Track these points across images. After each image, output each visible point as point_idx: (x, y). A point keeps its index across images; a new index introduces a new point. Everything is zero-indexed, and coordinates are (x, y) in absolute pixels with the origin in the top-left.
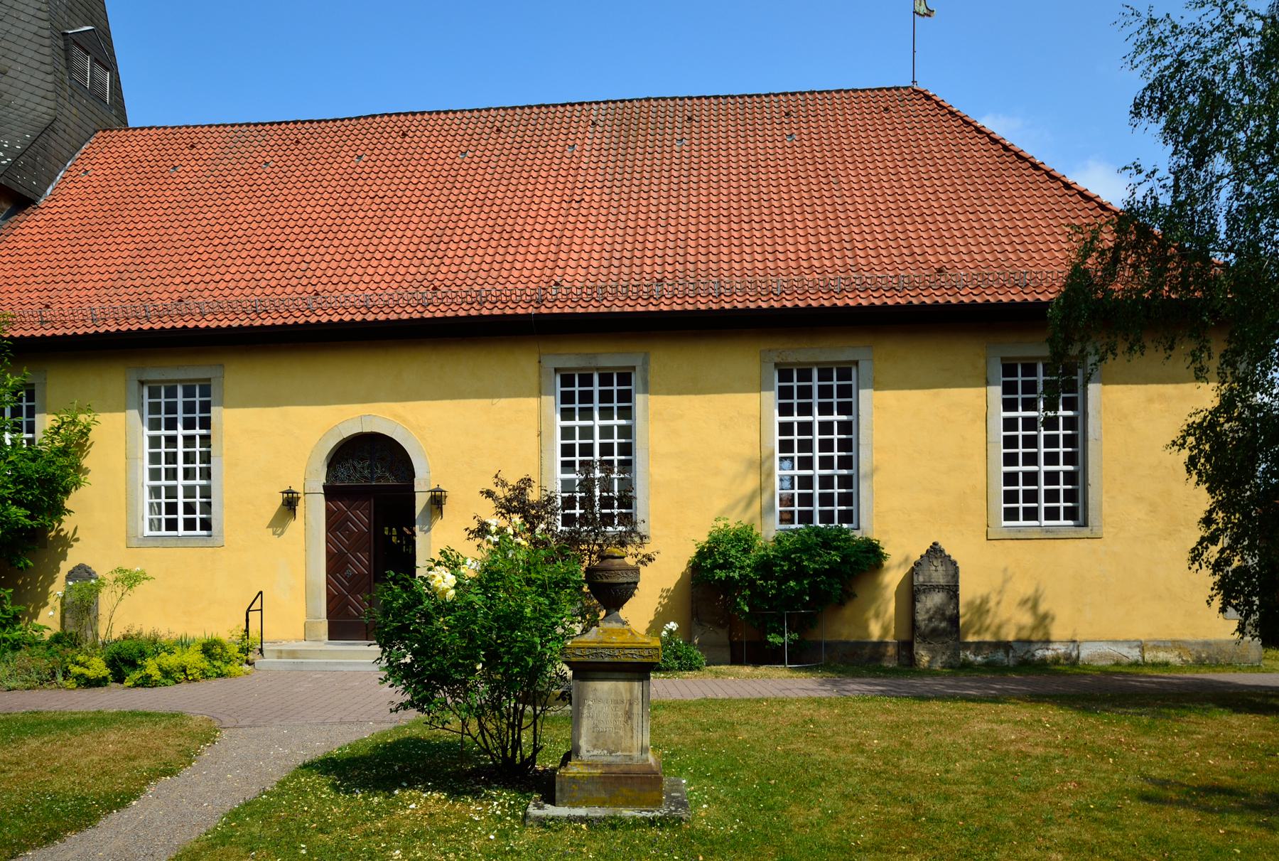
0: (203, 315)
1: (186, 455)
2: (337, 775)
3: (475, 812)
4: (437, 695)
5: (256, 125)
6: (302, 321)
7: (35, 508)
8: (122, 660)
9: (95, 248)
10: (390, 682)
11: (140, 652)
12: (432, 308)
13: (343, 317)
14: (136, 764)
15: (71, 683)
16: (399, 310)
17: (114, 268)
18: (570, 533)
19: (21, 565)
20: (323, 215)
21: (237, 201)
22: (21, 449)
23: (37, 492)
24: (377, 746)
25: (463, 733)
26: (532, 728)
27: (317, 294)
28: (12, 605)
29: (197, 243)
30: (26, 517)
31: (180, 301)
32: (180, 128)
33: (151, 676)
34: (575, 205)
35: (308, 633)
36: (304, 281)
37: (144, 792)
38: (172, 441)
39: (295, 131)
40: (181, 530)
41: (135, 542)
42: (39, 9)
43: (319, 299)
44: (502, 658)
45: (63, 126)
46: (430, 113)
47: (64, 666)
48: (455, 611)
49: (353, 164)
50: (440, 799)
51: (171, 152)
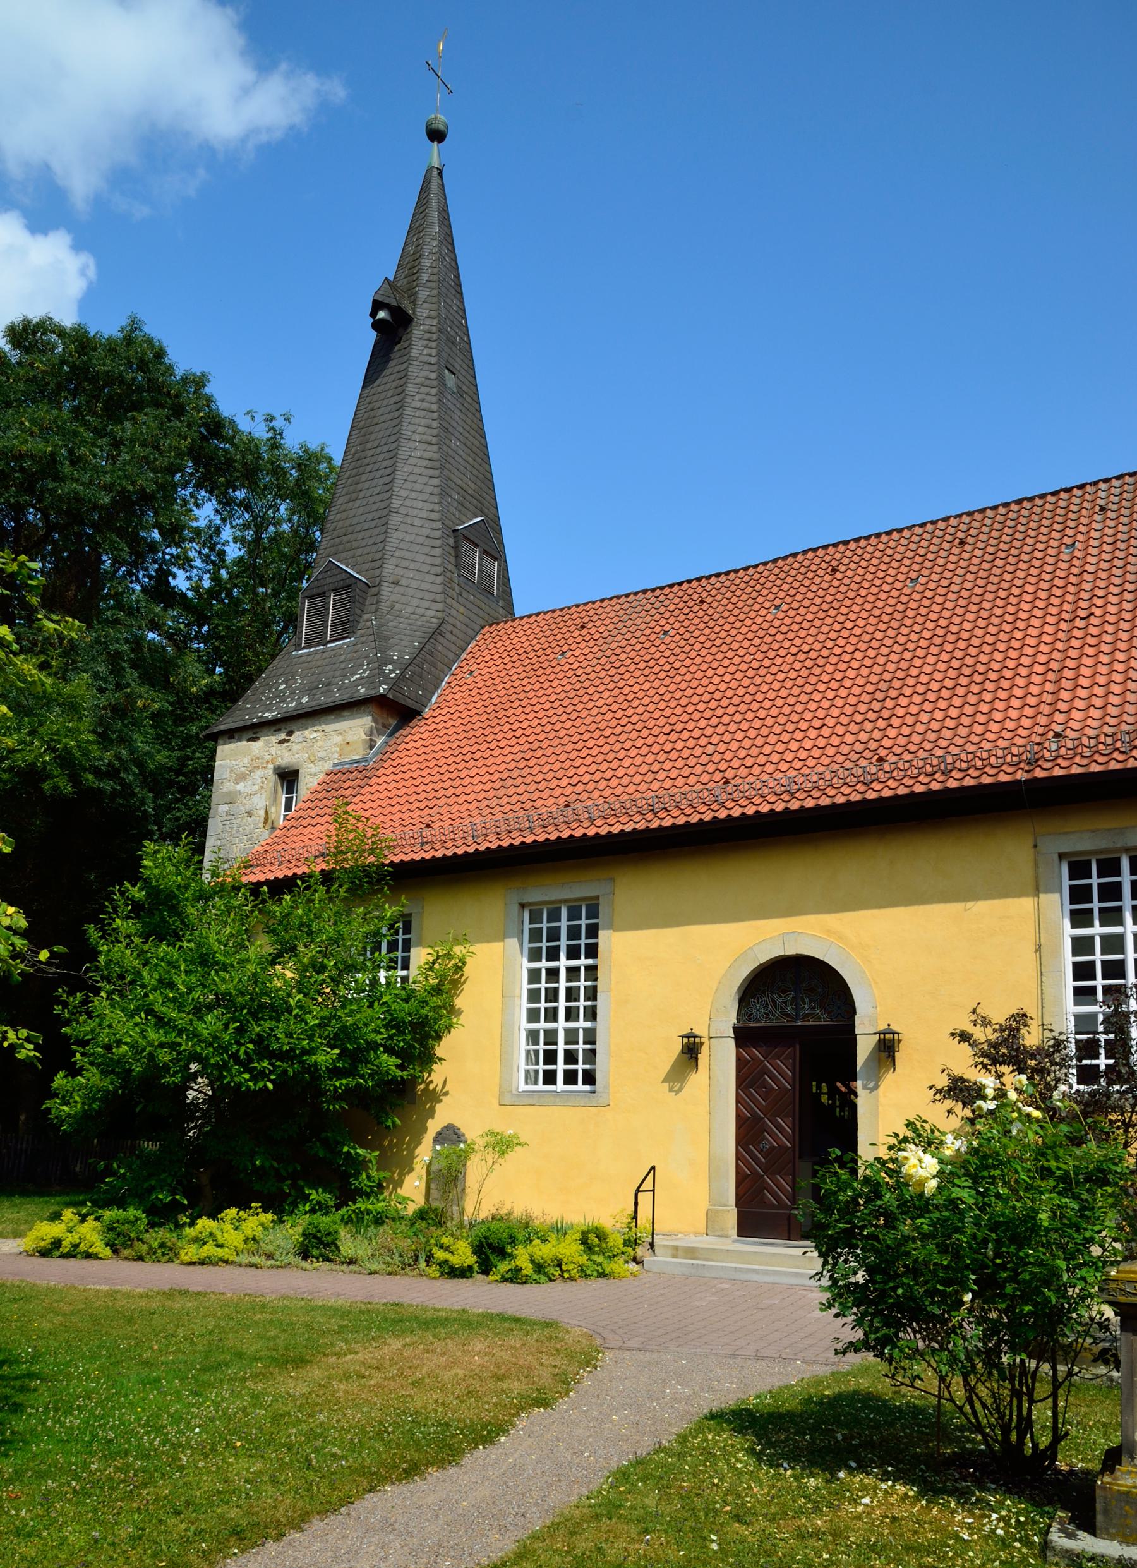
0: (592, 820)
1: (569, 990)
2: (756, 1436)
3: (962, 1524)
4: (901, 1335)
5: (653, 590)
6: (708, 817)
7: (406, 1057)
8: (490, 1246)
9: (478, 755)
10: (835, 1310)
11: (511, 1237)
12: (877, 786)
13: (760, 808)
14: (505, 1385)
15: (434, 1271)
16: (832, 792)
17: (497, 775)
18: (1092, 1094)
19: (389, 1123)
20: (734, 684)
21: (631, 681)
22: (395, 988)
23: (408, 1038)
24: (810, 1399)
25: (939, 1397)
26: (1050, 1400)
27: (727, 782)
28: (377, 1170)
29: (586, 736)
30: (397, 1066)
31: (567, 806)
32: (569, 608)
33: (521, 1269)
34: (1079, 623)
35: (711, 1225)
36: (711, 768)
37: (514, 1426)
38: (553, 974)
39: (699, 590)
40: (560, 1085)
41: (509, 1098)
42: (432, 511)
43: (730, 789)
44: (1003, 1287)
45: (450, 628)
46: (868, 538)
47: (428, 1248)
48: (928, 1211)
49: (769, 618)
50: (906, 1494)
51: (559, 637)
